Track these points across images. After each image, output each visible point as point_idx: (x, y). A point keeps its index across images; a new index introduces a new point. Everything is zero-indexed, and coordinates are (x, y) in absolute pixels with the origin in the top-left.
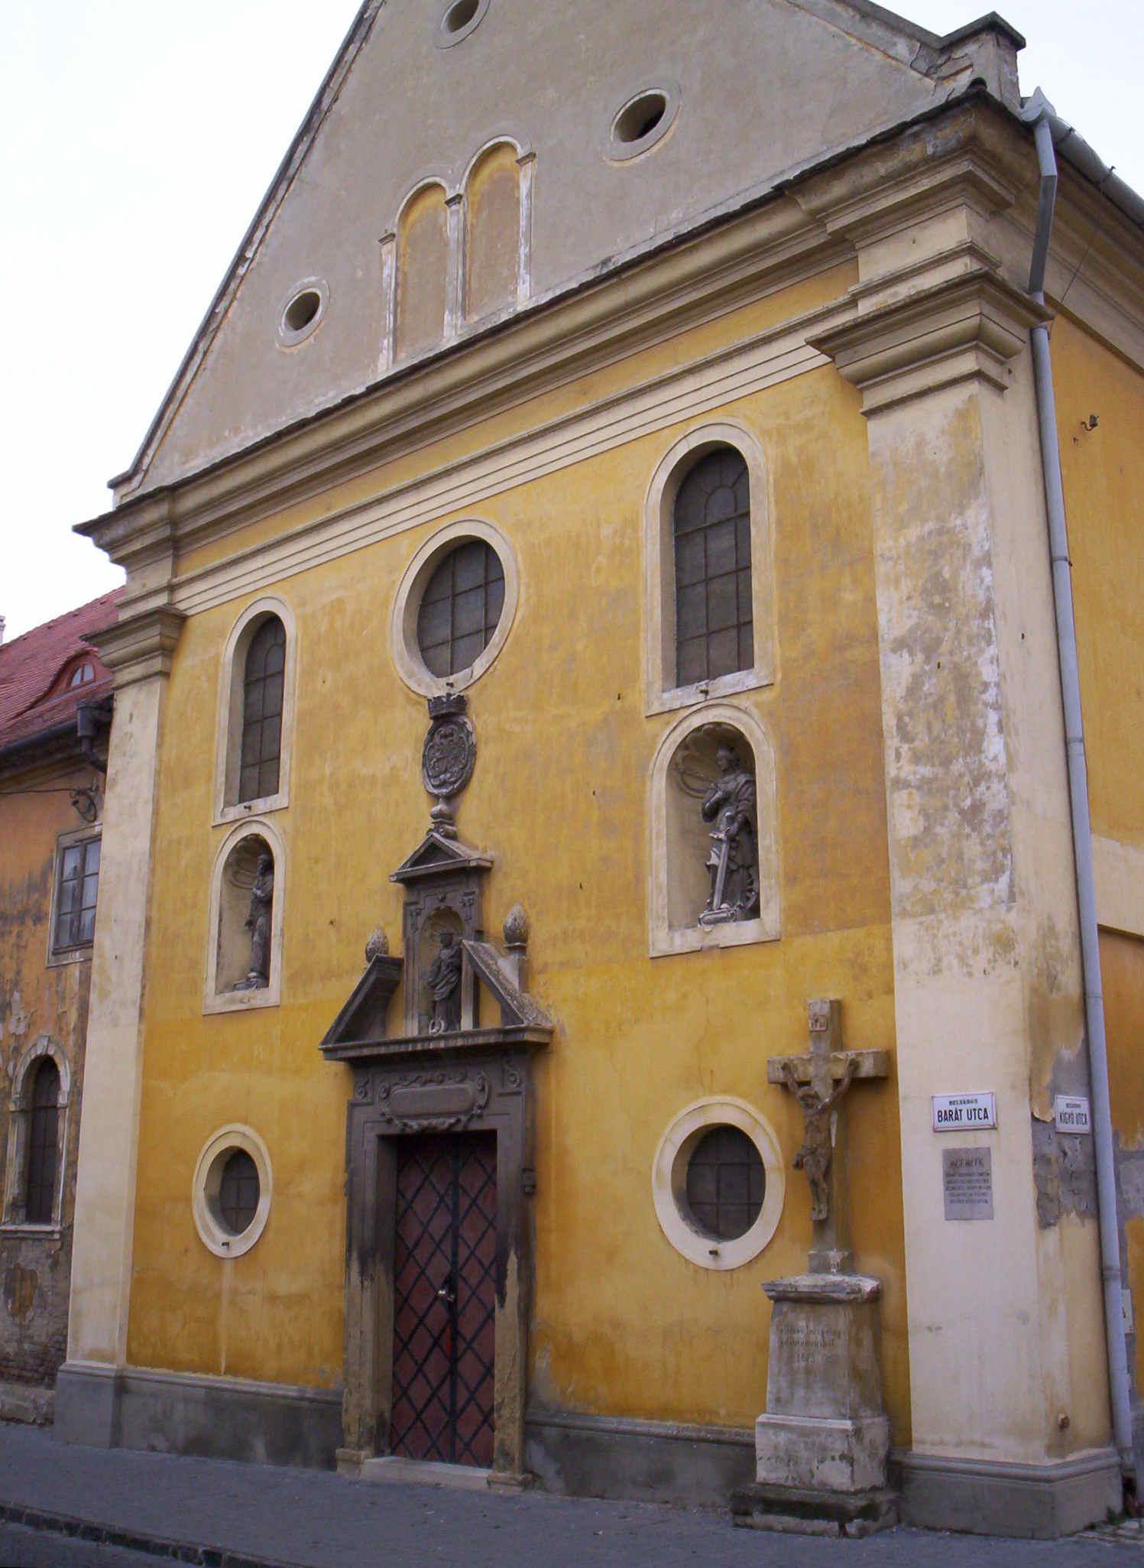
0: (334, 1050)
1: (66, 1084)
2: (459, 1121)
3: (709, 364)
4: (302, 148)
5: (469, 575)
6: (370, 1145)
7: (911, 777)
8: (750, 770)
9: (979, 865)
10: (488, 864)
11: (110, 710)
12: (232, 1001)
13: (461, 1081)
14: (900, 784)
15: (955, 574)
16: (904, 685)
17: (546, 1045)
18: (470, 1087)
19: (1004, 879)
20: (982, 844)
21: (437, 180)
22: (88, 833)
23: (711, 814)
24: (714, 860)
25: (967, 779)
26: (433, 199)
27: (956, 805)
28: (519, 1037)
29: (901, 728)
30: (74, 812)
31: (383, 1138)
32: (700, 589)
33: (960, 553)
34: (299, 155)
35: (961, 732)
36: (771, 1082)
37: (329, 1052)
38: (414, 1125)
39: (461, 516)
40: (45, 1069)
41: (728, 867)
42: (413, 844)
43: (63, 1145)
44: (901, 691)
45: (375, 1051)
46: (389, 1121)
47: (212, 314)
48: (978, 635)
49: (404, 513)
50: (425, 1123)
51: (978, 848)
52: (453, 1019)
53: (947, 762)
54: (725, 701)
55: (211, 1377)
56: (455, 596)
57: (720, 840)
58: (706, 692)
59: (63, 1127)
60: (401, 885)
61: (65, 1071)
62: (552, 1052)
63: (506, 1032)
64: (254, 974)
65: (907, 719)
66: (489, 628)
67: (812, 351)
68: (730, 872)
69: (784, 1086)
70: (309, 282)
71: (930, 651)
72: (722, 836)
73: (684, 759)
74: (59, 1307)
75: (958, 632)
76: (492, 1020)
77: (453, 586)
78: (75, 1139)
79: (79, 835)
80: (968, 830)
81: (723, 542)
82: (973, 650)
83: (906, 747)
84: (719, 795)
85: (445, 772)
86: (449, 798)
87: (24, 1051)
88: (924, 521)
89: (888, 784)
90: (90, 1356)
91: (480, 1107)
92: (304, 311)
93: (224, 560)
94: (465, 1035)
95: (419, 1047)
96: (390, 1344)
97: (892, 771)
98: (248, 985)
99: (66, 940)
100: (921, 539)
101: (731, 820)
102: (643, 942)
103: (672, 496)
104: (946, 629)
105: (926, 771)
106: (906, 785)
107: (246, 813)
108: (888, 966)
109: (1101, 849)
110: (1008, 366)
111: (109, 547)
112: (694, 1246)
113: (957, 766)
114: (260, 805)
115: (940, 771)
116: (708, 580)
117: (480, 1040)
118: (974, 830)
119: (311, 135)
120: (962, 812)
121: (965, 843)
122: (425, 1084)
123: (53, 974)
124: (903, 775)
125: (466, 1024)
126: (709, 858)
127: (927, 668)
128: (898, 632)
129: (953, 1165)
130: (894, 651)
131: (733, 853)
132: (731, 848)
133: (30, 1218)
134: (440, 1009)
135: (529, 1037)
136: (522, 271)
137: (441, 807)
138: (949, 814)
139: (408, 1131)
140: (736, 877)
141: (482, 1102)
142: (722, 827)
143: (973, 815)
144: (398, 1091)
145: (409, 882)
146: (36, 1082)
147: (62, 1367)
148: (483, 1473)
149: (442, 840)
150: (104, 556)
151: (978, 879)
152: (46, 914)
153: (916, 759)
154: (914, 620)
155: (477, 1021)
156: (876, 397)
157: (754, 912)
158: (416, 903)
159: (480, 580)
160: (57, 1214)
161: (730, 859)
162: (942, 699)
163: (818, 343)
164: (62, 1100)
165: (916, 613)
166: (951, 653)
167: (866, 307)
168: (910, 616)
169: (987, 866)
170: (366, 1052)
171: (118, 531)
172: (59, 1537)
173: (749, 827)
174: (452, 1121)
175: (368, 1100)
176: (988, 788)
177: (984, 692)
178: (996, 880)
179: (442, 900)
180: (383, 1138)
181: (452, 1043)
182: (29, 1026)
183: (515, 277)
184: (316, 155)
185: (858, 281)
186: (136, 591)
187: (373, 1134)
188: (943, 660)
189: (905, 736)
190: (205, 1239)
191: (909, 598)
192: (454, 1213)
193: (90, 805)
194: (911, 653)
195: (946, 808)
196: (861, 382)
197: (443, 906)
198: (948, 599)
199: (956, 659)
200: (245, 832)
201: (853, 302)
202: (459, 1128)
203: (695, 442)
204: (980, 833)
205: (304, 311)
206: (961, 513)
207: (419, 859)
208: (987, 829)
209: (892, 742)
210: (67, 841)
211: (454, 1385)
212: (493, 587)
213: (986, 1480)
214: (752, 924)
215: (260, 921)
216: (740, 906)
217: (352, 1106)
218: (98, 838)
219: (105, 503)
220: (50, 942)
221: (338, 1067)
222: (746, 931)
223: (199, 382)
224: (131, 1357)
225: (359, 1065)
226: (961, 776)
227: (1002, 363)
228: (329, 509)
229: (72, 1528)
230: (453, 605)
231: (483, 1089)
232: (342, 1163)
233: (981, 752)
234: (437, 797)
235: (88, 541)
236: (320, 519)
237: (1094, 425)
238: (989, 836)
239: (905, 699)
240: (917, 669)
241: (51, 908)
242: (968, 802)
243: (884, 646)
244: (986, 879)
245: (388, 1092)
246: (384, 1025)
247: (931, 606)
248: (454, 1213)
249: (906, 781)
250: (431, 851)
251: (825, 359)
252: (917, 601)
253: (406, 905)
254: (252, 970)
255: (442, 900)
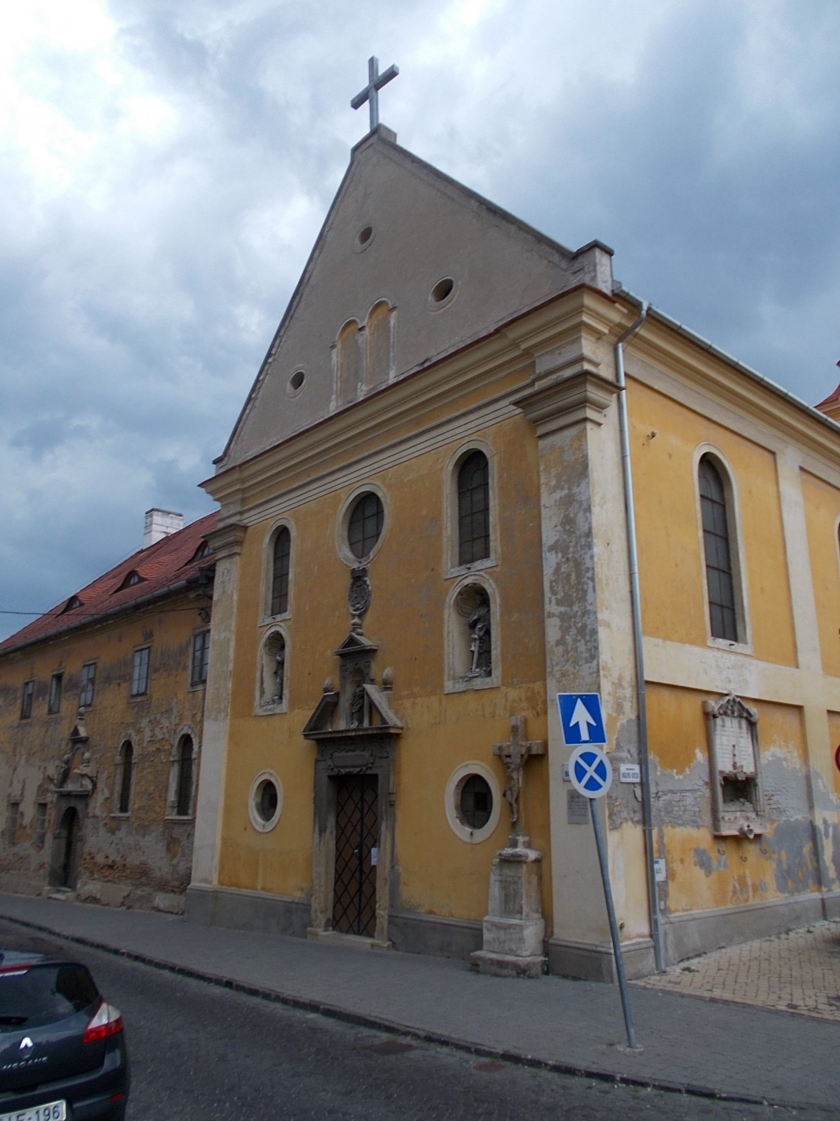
0: (308, 735)
1: (195, 748)
2: (362, 770)
3: (471, 412)
4: (297, 300)
5: (370, 510)
6: (325, 779)
7: (555, 612)
8: (488, 606)
9: (584, 655)
10: (376, 648)
11: (214, 571)
12: (266, 710)
13: (363, 750)
14: (551, 615)
15: (576, 515)
16: (553, 568)
17: (400, 734)
18: (367, 754)
19: (595, 662)
20: (586, 645)
21: (355, 318)
22: (206, 629)
23: (473, 626)
24: (473, 649)
25: (579, 613)
26: (352, 328)
27: (575, 625)
28: (387, 731)
29: (552, 588)
30: (199, 619)
31: (330, 777)
32: (469, 518)
33: (578, 505)
34: (295, 303)
35: (577, 590)
36: (494, 755)
37: (306, 736)
38: (343, 771)
39: (366, 481)
40: (186, 741)
41: (479, 651)
42: (344, 639)
43: (194, 779)
44: (551, 571)
45: (325, 736)
46: (333, 769)
47: (257, 381)
48: (585, 545)
49: (341, 480)
50: (347, 770)
51: (584, 647)
52: (361, 721)
53: (571, 605)
54: (477, 573)
55: (254, 891)
56: (364, 519)
57: (475, 639)
58: (469, 568)
59: (194, 768)
60: (339, 657)
61: (195, 741)
62: (402, 738)
63: (381, 728)
64: (276, 697)
65: (554, 584)
66: (378, 535)
67: (513, 407)
68: (480, 654)
69: (500, 756)
70: (299, 367)
71: (564, 553)
72: (476, 637)
73: (461, 599)
74: (188, 853)
75: (577, 543)
76: (377, 723)
77: (363, 514)
78: (198, 774)
79: (202, 630)
80: (579, 638)
81: (478, 496)
82: (583, 552)
83: (553, 597)
84: (476, 617)
85: (358, 604)
86: (360, 616)
87: (178, 731)
88: (563, 489)
89: (546, 614)
90: (201, 881)
91: (371, 763)
92: (298, 380)
93: (263, 500)
94: (367, 729)
95: (344, 735)
96: (333, 875)
97: (547, 608)
98: (274, 701)
99: (196, 679)
100: (561, 498)
101: (481, 629)
102: (442, 686)
103: (456, 475)
104: (571, 542)
105: (563, 609)
106: (554, 615)
107: (272, 621)
108: (545, 702)
109: (648, 644)
110: (603, 414)
111: (211, 493)
112: (463, 832)
113: (575, 608)
114: (279, 617)
115: (568, 609)
116: (472, 514)
117: (370, 732)
118: (582, 637)
119: (300, 295)
120: (577, 629)
121: (578, 644)
122: (348, 751)
123: (191, 695)
124: (552, 611)
125: (366, 724)
126: (471, 647)
127: (563, 560)
128: (551, 542)
129: (572, 797)
130: (549, 551)
131: (481, 645)
132: (480, 643)
133: (179, 813)
134: (355, 716)
135: (392, 731)
136: (391, 364)
137: (356, 620)
138: (572, 630)
139: (340, 774)
140: (483, 656)
141: (372, 761)
142: (477, 632)
143: (582, 631)
144: (337, 754)
145: (342, 656)
146: (184, 746)
147: (189, 886)
148: (369, 941)
149: (356, 636)
150: (210, 497)
151: (584, 661)
152: (188, 666)
153: (559, 603)
154: (558, 537)
155: (371, 723)
156: (541, 430)
157: (489, 674)
158: (345, 665)
159: (374, 512)
160: (190, 811)
161: (480, 647)
162: (569, 575)
163: (516, 403)
164: (194, 756)
165: (558, 534)
166: (574, 553)
167: (538, 386)
168: (556, 535)
169: (588, 655)
170: (321, 736)
171: (213, 487)
172: (166, 973)
173: (488, 632)
174: (359, 769)
175: (324, 758)
176: (589, 618)
177: (587, 572)
178: (591, 662)
179: (356, 664)
180: (330, 777)
181: (358, 733)
182: (180, 719)
183: (388, 366)
184: (302, 305)
185: (535, 372)
186: (225, 514)
187: (326, 774)
188: (570, 556)
189: (554, 592)
190: (254, 825)
191: (556, 526)
192: (362, 812)
193: (206, 614)
194: (556, 553)
195: (570, 627)
196: (536, 422)
197: (356, 667)
198: (572, 527)
199: (576, 556)
200: (273, 630)
201: (532, 384)
202: (362, 773)
203: (464, 449)
204: (585, 639)
205: (298, 380)
206: (578, 486)
207: (346, 645)
208: (588, 638)
209: (548, 594)
210: (197, 631)
211: (360, 896)
212: (380, 515)
213: (586, 954)
214: (488, 679)
215: (280, 672)
216: (485, 671)
217: (317, 761)
218: (209, 631)
219: (211, 472)
220: (189, 680)
221: (309, 743)
222: (487, 682)
223: (253, 414)
224: (220, 882)
225: (319, 742)
226: (577, 612)
227: (600, 412)
228: (309, 476)
229: (172, 969)
230: (364, 523)
231: (372, 755)
232: (312, 789)
233: (586, 601)
234: (354, 616)
235: (203, 490)
236: (305, 481)
237: (653, 437)
238: (589, 641)
239: (554, 574)
240: (558, 560)
241: (190, 664)
242: (580, 624)
243: (545, 549)
244: (587, 662)
245: (332, 754)
246: (332, 724)
247: (565, 530)
248: (362, 812)
249: (553, 613)
250: (352, 641)
251: (520, 410)
252: (559, 528)
253: (342, 666)
254: (276, 695)
255: (356, 664)
